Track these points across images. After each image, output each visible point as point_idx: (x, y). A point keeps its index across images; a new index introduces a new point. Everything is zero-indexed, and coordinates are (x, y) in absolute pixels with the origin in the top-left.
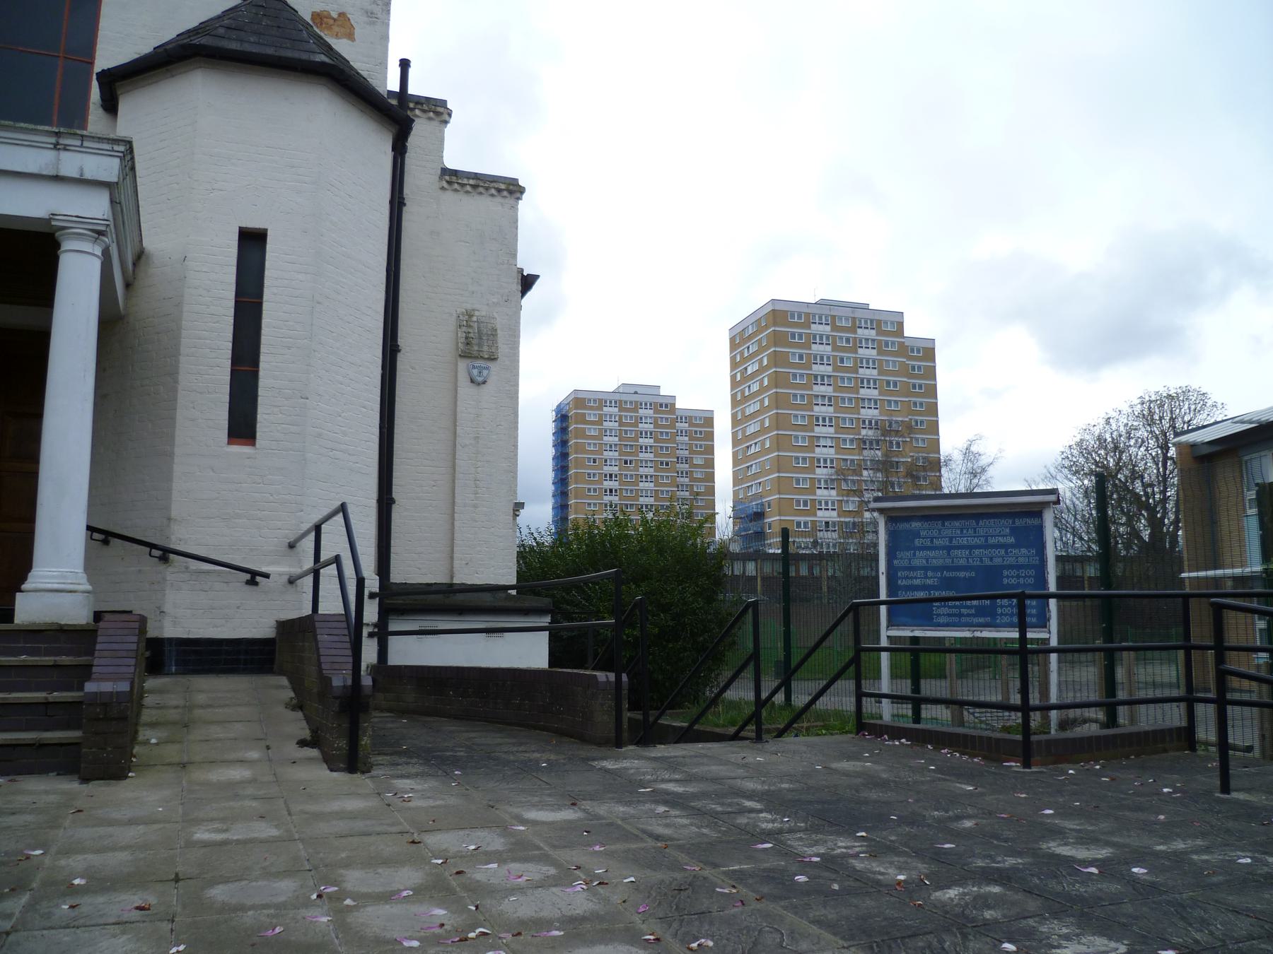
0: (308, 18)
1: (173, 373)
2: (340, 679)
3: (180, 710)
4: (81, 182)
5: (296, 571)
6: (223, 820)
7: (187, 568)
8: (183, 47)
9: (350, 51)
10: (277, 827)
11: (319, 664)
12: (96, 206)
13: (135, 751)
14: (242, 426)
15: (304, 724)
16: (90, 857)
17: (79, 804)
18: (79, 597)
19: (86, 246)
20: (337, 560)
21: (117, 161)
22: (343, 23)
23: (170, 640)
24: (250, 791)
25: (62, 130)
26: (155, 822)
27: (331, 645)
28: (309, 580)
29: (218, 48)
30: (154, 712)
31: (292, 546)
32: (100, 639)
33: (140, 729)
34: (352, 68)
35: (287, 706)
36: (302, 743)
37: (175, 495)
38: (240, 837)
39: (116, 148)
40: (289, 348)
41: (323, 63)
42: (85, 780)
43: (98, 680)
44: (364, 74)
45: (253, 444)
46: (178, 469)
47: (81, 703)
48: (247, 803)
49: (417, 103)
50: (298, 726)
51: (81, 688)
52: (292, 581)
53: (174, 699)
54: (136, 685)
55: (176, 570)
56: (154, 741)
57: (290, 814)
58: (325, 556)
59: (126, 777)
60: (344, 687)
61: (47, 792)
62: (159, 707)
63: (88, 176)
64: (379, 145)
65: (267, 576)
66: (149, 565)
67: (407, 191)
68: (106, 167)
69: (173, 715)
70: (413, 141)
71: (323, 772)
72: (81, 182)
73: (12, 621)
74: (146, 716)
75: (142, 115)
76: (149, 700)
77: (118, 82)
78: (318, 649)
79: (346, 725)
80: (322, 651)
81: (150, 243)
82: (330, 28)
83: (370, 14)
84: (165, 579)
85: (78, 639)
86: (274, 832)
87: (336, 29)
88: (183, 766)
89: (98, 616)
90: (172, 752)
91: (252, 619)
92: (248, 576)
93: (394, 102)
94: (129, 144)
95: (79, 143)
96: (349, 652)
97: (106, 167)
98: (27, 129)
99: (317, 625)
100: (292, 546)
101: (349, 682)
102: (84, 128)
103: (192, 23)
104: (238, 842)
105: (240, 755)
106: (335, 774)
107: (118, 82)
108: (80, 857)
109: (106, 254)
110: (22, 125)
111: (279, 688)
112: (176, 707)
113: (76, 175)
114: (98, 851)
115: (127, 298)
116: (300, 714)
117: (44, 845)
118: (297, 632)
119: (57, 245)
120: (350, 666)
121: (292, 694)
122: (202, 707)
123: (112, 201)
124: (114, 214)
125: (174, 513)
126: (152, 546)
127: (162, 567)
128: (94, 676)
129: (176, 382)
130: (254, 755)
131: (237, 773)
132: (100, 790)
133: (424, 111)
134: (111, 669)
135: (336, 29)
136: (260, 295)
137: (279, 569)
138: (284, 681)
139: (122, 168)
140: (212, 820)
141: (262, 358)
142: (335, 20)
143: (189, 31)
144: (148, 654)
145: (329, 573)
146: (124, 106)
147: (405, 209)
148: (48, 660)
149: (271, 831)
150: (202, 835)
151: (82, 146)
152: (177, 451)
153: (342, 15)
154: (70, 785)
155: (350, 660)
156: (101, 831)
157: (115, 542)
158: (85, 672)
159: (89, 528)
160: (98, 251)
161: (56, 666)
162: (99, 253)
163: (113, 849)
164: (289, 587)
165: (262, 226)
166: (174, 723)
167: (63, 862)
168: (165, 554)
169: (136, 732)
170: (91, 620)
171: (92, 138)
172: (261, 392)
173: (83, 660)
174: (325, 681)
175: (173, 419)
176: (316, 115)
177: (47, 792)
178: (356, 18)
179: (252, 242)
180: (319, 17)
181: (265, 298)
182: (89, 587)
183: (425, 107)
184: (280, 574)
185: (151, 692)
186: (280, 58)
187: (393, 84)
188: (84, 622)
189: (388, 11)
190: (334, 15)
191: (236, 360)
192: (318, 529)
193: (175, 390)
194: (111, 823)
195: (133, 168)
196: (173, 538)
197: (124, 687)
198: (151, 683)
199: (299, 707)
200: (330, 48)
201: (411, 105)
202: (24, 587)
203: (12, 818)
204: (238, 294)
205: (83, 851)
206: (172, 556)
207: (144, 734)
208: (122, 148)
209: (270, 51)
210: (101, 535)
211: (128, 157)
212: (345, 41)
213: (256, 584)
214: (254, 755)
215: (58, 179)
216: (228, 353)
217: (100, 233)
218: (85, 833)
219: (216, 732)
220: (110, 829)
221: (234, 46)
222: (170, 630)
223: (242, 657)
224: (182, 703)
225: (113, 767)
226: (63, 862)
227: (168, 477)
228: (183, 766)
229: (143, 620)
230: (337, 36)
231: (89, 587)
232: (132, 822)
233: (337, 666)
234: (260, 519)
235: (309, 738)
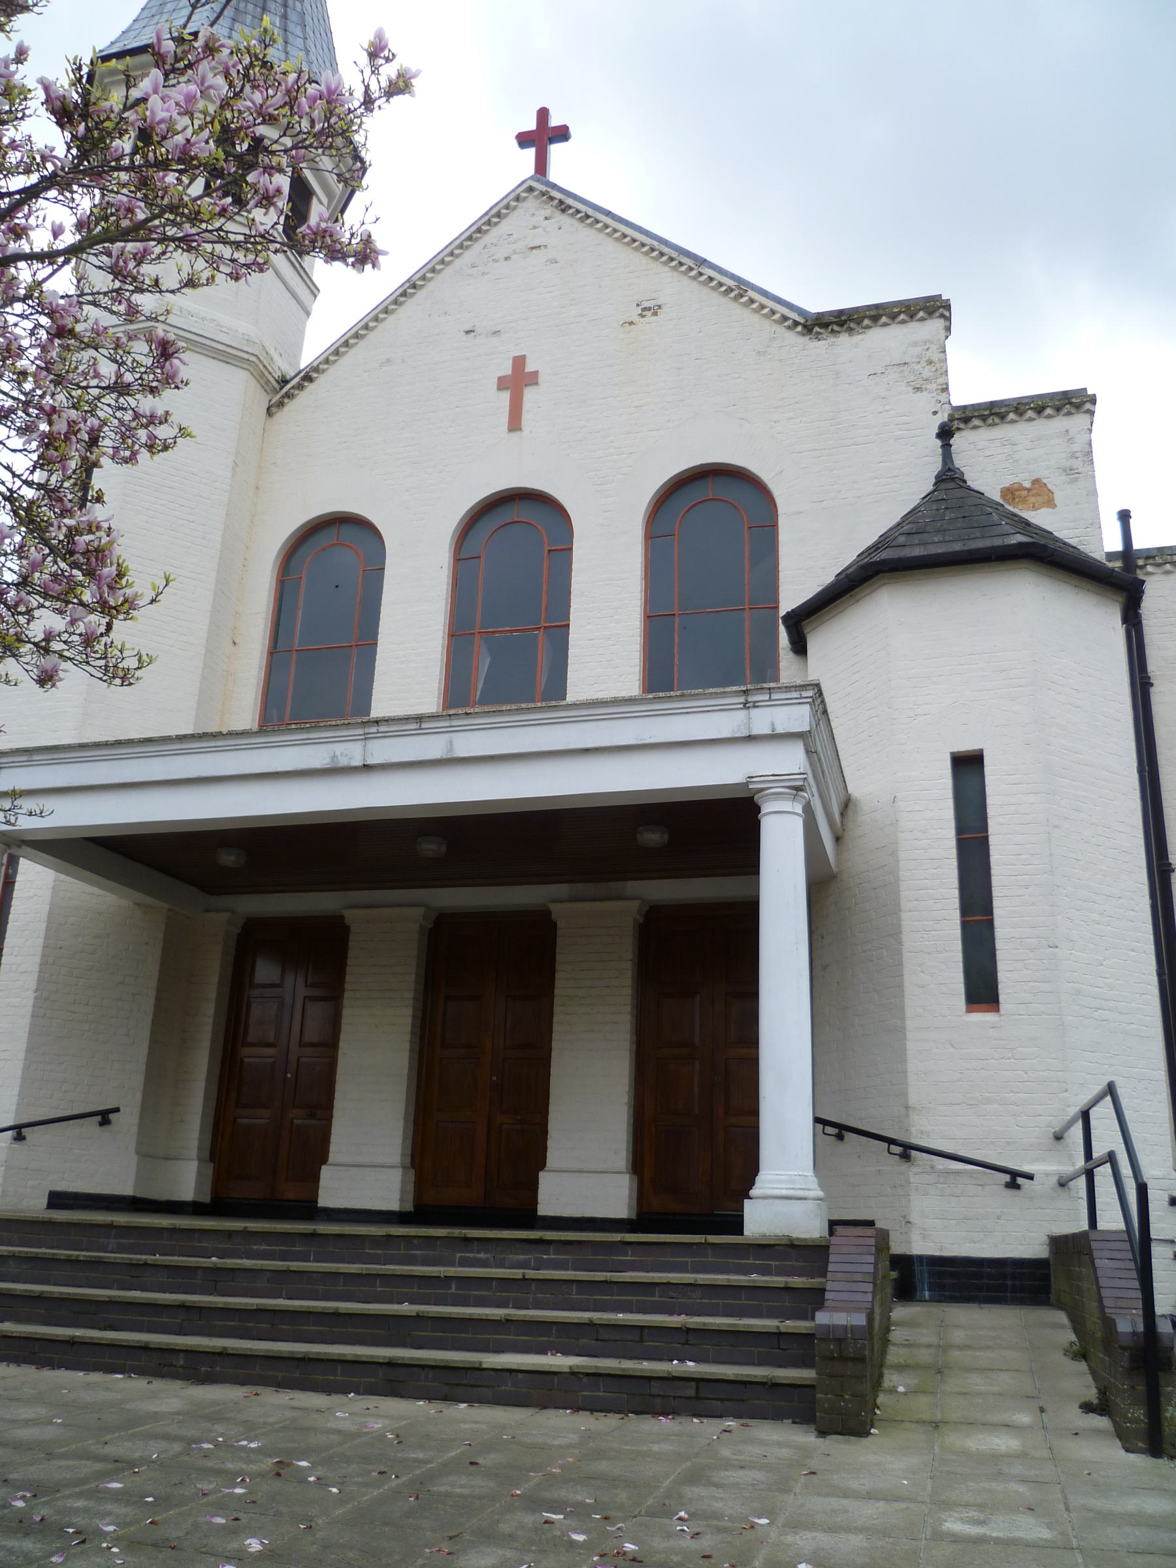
0: (997, 497)
1: (896, 934)
2: (1128, 1324)
3: (932, 1350)
4: (775, 737)
5: (1067, 1169)
6: (981, 1507)
7: (932, 1167)
8: (863, 567)
9: (1053, 521)
10: (1049, 1526)
11: (1100, 1299)
12: (790, 761)
13: (879, 1401)
14: (982, 990)
15: (1089, 1379)
16: (820, 1536)
17: (813, 1464)
18: (811, 1205)
19: (785, 805)
20: (1111, 1158)
21: (807, 708)
22: (1040, 492)
23: (921, 1258)
24: (1018, 1469)
25: (749, 687)
26: (897, 1499)
27: (1113, 1271)
28: (1082, 1182)
29: (900, 560)
30: (902, 1351)
31: (1058, 1137)
32: (832, 1258)
33: (886, 1372)
34: (1057, 540)
35: (1066, 1352)
36: (1087, 1408)
37: (912, 1079)
38: (1001, 1535)
39: (805, 694)
40: (1027, 887)
41: (1021, 545)
42: (822, 1433)
43: (836, 1309)
44: (1073, 542)
45: (997, 1010)
46: (912, 1047)
47: (813, 1335)
48: (1014, 1486)
49: (1148, 558)
50: (1080, 1382)
51: (813, 1319)
52: (1063, 1184)
53: (926, 1336)
54: (877, 1318)
55: (920, 1169)
56: (901, 1389)
57: (1067, 1509)
58: (1098, 1151)
59: (868, 1434)
60: (1134, 1333)
61: (779, 1444)
62: (909, 1345)
63: (780, 730)
64: (1102, 621)
65: (1030, 1177)
66: (890, 1163)
67: (1153, 667)
68: (796, 717)
69: (924, 1356)
70: (1148, 606)
71: (1115, 1452)
72: (775, 737)
73: (742, 1234)
74: (894, 1355)
75: (835, 651)
76: (896, 1335)
77: (801, 623)
78: (1097, 1278)
79: (1141, 1388)
80: (1103, 1282)
81: (855, 789)
82: (1024, 500)
83: (1069, 471)
84: (908, 1182)
85: (809, 1255)
86: (1045, 1534)
87: (1032, 500)
88: (936, 1425)
89: (833, 1224)
90: (922, 1406)
91: (1015, 1233)
92: (1007, 1178)
93: (1117, 565)
94: (817, 687)
95: (767, 697)
96: (1136, 1284)
97: (796, 717)
98: (716, 693)
99: (1094, 1245)
100: (1058, 1137)
101: (1141, 1328)
102: (776, 679)
103: (872, 539)
104: (998, 1541)
105: (1005, 1417)
106: (1132, 1456)
107: (801, 623)
108: (809, 1535)
109: (808, 811)
110: (711, 690)
111: (1054, 1327)
112: (929, 1346)
113: (768, 731)
114: (830, 1530)
115: (838, 853)
116: (1083, 1366)
117: (770, 1513)
118: (1071, 1250)
119: (758, 809)
120: (1140, 1304)
121: (1073, 1337)
122: (959, 1348)
123: (808, 752)
124: (812, 764)
125: (913, 1100)
126: (891, 1141)
127: (904, 1166)
128: (826, 1304)
129: (900, 943)
130: (1024, 1418)
131: (1004, 1443)
132: (837, 1446)
133: (1158, 565)
134: (845, 1296)
135: (1032, 500)
136: (985, 828)
137: (1045, 1167)
138: (1062, 1317)
139: (814, 713)
140: (967, 1505)
141: (995, 903)
142: (1029, 490)
143: (869, 548)
144: (894, 1275)
145: (1103, 1174)
146: (814, 645)
147: (1152, 690)
148: (779, 1281)
149: (1040, 1532)
150: (953, 1525)
151: (770, 700)
152: (910, 1024)
153: (1036, 482)
154: (806, 1437)
155: (1139, 1294)
156: (835, 1503)
157: (849, 1136)
158: (815, 1299)
159: (817, 1120)
160: (798, 808)
161: (787, 1289)
162: (800, 811)
163: (848, 1530)
164: (1060, 1190)
165: (976, 747)
166: (927, 1367)
167: (789, 1539)
168: (907, 1151)
169: (881, 1376)
170: (826, 1233)
171: (788, 689)
172: (999, 944)
173: (815, 1282)
174: (1109, 1324)
175: (901, 986)
176: (1022, 606)
177: (779, 1444)
178: (1054, 481)
179: (968, 765)
180: (1010, 493)
181: (991, 830)
182: (821, 1194)
183: (1159, 560)
184: (1047, 1175)
185: (898, 1324)
186: (970, 551)
187: (1113, 542)
188: (816, 1235)
189: (1091, 462)
190: (1027, 485)
191: (988, 909)
192: (1085, 1115)
193: (899, 953)
194: (847, 1494)
195: (825, 712)
196: (913, 1130)
197: (860, 1320)
198: (900, 1312)
199: (1082, 1355)
200: (1027, 523)
201: (1140, 562)
202: (752, 1193)
203: (741, 1473)
204: (960, 830)
205: (812, 1526)
206: (914, 1153)
207: (891, 1379)
208: (810, 693)
209: (957, 547)
210: (832, 1129)
211: (819, 700)
212: (1044, 510)
213: (1018, 1187)
214: (1024, 1418)
215: (751, 739)
216: (955, 902)
217: (798, 789)
218: (818, 1504)
219: (976, 1382)
220: (845, 1502)
221: (918, 552)
222: (920, 1247)
223: (1009, 1283)
224: (934, 1340)
225: (851, 1420)
226: (789, 1539)
227: (903, 1059)
228: (936, 1425)
229: (883, 1237)
230: (1034, 508)
231: (821, 1194)
232: (871, 1496)
233: (1124, 1304)
234: (1015, 1104)
235: (1095, 1401)
